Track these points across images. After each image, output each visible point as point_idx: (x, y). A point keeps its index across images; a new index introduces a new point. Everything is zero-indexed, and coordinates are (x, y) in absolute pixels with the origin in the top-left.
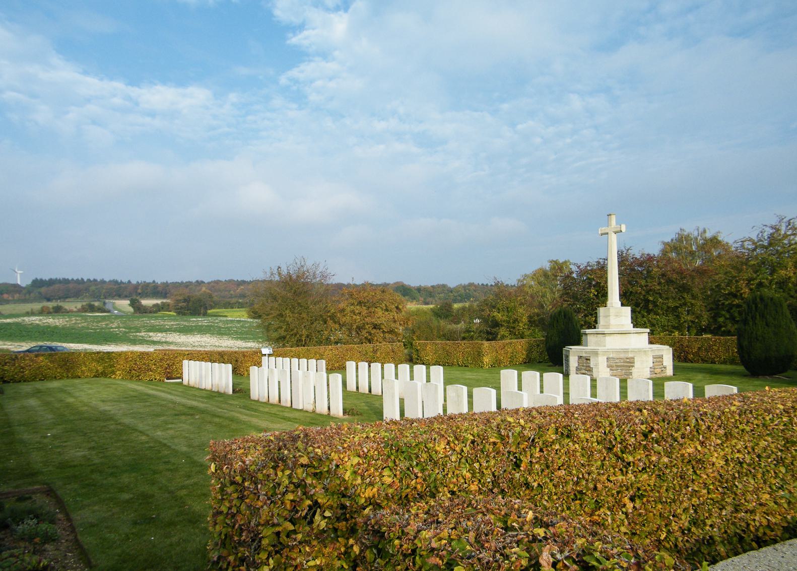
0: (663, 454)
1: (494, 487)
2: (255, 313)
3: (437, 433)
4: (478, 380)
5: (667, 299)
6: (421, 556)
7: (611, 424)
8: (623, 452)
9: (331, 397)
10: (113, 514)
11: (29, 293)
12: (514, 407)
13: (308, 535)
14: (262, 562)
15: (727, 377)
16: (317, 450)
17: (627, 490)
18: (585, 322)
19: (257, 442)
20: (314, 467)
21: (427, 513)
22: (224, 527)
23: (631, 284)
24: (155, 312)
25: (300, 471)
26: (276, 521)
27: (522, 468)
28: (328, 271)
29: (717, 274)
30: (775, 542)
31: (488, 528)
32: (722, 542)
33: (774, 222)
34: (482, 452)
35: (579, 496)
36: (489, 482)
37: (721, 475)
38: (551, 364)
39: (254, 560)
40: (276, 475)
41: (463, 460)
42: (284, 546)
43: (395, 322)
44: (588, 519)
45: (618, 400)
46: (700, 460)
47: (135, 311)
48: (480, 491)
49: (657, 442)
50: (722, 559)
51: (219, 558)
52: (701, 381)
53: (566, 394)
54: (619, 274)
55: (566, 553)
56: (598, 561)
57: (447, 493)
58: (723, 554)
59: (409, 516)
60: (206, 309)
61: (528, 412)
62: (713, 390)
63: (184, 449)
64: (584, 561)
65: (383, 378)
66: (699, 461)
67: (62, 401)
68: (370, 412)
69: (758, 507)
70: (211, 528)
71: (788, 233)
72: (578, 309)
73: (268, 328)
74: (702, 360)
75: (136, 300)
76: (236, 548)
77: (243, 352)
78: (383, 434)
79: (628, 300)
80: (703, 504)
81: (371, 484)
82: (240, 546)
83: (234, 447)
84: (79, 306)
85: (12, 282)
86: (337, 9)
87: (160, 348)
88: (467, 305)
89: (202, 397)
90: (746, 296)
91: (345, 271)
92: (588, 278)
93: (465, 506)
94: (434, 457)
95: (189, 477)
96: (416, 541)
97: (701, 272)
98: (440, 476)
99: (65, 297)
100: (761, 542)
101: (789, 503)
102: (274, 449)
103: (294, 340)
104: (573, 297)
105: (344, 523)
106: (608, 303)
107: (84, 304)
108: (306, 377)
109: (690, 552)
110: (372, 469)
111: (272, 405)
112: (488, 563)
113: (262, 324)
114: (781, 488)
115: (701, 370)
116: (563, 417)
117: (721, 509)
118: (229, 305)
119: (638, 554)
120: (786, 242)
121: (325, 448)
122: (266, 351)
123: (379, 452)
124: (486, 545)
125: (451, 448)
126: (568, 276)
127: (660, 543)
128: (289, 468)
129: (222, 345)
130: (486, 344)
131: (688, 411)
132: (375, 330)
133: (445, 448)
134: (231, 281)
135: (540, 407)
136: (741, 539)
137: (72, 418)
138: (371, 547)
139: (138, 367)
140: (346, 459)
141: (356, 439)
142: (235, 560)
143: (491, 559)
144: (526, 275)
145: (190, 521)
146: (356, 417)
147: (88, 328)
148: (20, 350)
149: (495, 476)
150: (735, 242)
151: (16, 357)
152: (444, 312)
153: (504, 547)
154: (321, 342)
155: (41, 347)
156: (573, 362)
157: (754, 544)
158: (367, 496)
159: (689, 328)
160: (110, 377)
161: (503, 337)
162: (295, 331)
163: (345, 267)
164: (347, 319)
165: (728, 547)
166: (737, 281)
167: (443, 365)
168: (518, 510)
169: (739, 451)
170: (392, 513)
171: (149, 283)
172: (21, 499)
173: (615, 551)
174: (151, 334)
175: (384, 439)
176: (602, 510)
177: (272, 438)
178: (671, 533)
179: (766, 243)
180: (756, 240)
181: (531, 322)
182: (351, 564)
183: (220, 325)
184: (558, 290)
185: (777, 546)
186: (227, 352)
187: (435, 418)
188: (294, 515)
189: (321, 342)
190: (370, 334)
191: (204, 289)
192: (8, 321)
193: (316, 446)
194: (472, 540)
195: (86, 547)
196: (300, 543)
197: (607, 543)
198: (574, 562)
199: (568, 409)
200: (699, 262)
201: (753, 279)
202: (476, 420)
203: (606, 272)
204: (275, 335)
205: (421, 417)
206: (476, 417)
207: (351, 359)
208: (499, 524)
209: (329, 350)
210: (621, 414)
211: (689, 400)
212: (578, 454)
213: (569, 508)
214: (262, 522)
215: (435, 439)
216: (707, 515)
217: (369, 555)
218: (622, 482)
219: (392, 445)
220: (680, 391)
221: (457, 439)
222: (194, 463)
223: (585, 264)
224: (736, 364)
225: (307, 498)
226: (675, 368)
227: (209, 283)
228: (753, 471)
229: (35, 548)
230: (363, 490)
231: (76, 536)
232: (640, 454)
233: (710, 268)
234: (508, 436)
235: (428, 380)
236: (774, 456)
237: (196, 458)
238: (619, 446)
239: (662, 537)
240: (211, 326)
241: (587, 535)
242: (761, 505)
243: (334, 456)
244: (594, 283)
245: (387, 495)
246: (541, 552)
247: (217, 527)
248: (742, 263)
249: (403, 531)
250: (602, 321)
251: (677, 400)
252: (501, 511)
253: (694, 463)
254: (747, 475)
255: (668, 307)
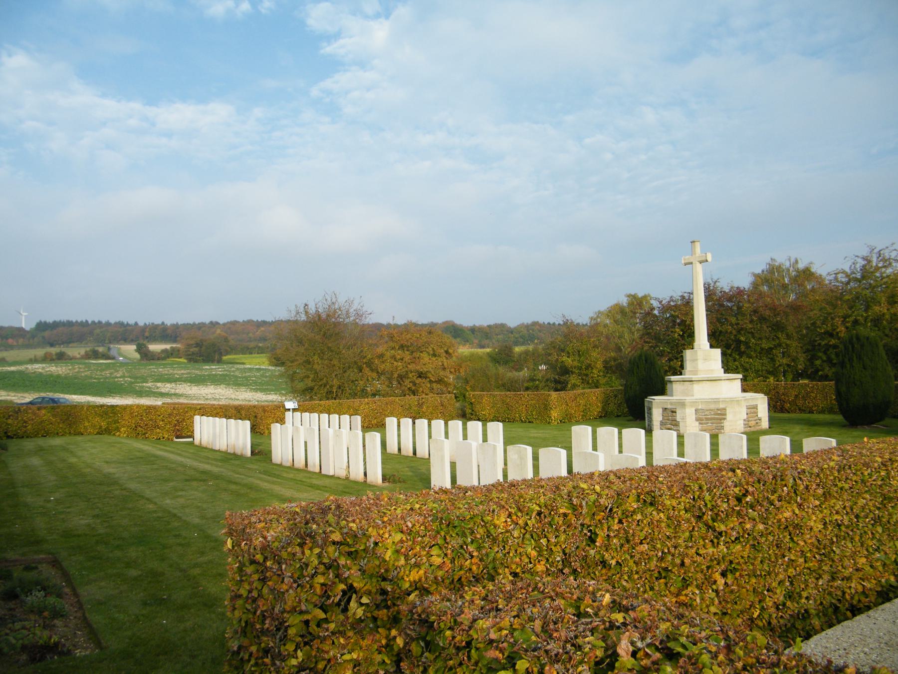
0: (758, 520)
1: (564, 566)
2: (278, 359)
3: (496, 503)
4: (544, 439)
5: (760, 339)
6: (477, 649)
7: (700, 488)
8: (714, 520)
9: (367, 460)
10: (121, 592)
11: (33, 337)
12: (588, 471)
13: (343, 625)
14: (289, 654)
15: (826, 429)
16: (351, 525)
17: (718, 564)
18: (670, 367)
19: (280, 514)
20: (348, 545)
21: (484, 599)
22: (244, 613)
23: (720, 322)
24: (164, 359)
25: (331, 549)
26: (304, 608)
27: (597, 544)
28: (364, 309)
29: (812, 310)
30: (869, 608)
31: (557, 615)
32: (817, 615)
33: (865, 252)
34: (551, 525)
35: (664, 573)
36: (558, 562)
37: (819, 541)
38: (631, 418)
39: (279, 651)
40: (303, 553)
41: (528, 536)
42: (314, 637)
43: (444, 369)
44: (674, 600)
45: (708, 459)
46: (797, 525)
47: (142, 358)
48: (548, 572)
49: (752, 507)
50: (817, 632)
51: (240, 648)
52: (798, 434)
53: (649, 454)
54: (707, 311)
55: (648, 641)
56: (684, 646)
57: (508, 575)
58: (818, 627)
59: (463, 603)
60: (221, 354)
61: (605, 476)
62: (812, 444)
63: (197, 521)
64: (668, 648)
65: (430, 437)
66: (797, 526)
67: (64, 460)
68: (416, 479)
69: (855, 572)
70: (229, 614)
71: (880, 265)
72: (661, 351)
73: (292, 378)
74: (800, 409)
75: (144, 345)
76: (258, 637)
77: (263, 407)
78: (431, 505)
79: (717, 341)
80: (799, 575)
81: (417, 565)
82: (263, 635)
83: (253, 519)
84: (83, 351)
85: (17, 325)
86: (377, 16)
87: (169, 400)
88: (531, 348)
89: (216, 460)
90: (842, 335)
91: (385, 308)
92: (672, 316)
93: (530, 590)
94: (492, 532)
95: (202, 553)
96: (471, 632)
97: (795, 308)
98: (500, 555)
99: (68, 342)
100: (855, 611)
101: (884, 565)
102: (300, 522)
103: (324, 391)
104: (655, 338)
105: (385, 611)
106: (696, 344)
107: (88, 349)
108: (338, 436)
109: (784, 629)
110: (418, 548)
111: (298, 470)
112: (556, 655)
113: (285, 372)
114: (877, 550)
115: (799, 422)
116: (646, 481)
117: (817, 579)
118: (248, 351)
119: (728, 636)
120: (878, 275)
121: (360, 522)
122: (290, 405)
123: (426, 527)
124: (555, 635)
125: (512, 521)
126: (649, 313)
127: (753, 622)
128: (318, 546)
129: (239, 397)
130: (554, 395)
131: (785, 470)
132: (420, 379)
133: (506, 521)
134: (250, 322)
135: (619, 470)
136: (836, 609)
137: (74, 480)
138: (417, 639)
139: (144, 423)
140: (387, 536)
141: (399, 511)
142: (258, 651)
143: (561, 651)
144: (600, 312)
145: (205, 605)
146: (398, 485)
147: (91, 378)
148: (23, 402)
149: (565, 554)
150: (829, 274)
151: (19, 410)
152: (503, 357)
153: (576, 637)
154: (356, 394)
155: (44, 398)
156: (657, 415)
157: (848, 613)
158: (412, 579)
159: (785, 372)
160: (114, 435)
161: (574, 387)
162: (324, 381)
163: (385, 304)
164: (387, 366)
165: (823, 619)
166: (833, 319)
167: (503, 421)
168: (593, 593)
169: (837, 513)
170: (443, 600)
171: (158, 325)
172: (28, 568)
173: (703, 634)
174: (159, 384)
175: (431, 511)
176: (690, 589)
177: (297, 510)
178: (765, 609)
179: (859, 276)
180: (849, 272)
181: (607, 368)
182: (394, 659)
183: (237, 373)
184: (638, 330)
185: (871, 613)
186: (245, 406)
187: (493, 485)
188: (326, 601)
189: (356, 394)
190: (415, 384)
191: (218, 331)
192: (13, 368)
193: (350, 519)
194: (538, 629)
195: (95, 626)
196: (333, 633)
197: (695, 626)
198: (657, 649)
199: (651, 471)
200: (792, 297)
201: (849, 316)
202: (542, 487)
203: (692, 308)
204: (301, 386)
205: (476, 484)
206: (543, 483)
207: (392, 414)
208: (570, 610)
209: (365, 403)
210: (712, 475)
211: (786, 456)
212: (663, 525)
213: (652, 589)
214: (288, 608)
215: (493, 511)
216: (803, 586)
217: (415, 648)
218: (713, 555)
219: (442, 518)
220: (776, 445)
221: (520, 510)
222: (208, 537)
223: (668, 299)
224: (835, 413)
225: (341, 581)
226: (771, 419)
227: (224, 324)
228: (851, 533)
229: (44, 622)
230: (407, 572)
231: (84, 614)
232: (733, 522)
233: (805, 304)
234: (581, 506)
235: (485, 439)
236: (872, 515)
237: (209, 532)
238: (710, 513)
239: (755, 616)
240: (227, 375)
241: (672, 619)
242: (857, 570)
243: (372, 532)
244: (678, 321)
245: (436, 578)
246: (619, 640)
247: (236, 612)
248: (837, 298)
249: (455, 621)
250: (688, 365)
251: (774, 457)
252: (573, 594)
253: (791, 529)
254: (844, 539)
255: (762, 349)
